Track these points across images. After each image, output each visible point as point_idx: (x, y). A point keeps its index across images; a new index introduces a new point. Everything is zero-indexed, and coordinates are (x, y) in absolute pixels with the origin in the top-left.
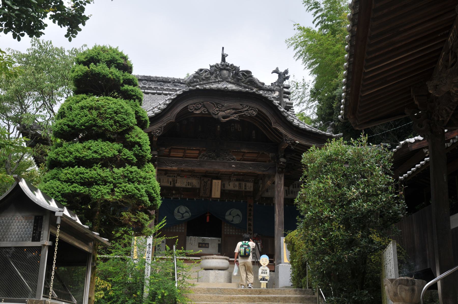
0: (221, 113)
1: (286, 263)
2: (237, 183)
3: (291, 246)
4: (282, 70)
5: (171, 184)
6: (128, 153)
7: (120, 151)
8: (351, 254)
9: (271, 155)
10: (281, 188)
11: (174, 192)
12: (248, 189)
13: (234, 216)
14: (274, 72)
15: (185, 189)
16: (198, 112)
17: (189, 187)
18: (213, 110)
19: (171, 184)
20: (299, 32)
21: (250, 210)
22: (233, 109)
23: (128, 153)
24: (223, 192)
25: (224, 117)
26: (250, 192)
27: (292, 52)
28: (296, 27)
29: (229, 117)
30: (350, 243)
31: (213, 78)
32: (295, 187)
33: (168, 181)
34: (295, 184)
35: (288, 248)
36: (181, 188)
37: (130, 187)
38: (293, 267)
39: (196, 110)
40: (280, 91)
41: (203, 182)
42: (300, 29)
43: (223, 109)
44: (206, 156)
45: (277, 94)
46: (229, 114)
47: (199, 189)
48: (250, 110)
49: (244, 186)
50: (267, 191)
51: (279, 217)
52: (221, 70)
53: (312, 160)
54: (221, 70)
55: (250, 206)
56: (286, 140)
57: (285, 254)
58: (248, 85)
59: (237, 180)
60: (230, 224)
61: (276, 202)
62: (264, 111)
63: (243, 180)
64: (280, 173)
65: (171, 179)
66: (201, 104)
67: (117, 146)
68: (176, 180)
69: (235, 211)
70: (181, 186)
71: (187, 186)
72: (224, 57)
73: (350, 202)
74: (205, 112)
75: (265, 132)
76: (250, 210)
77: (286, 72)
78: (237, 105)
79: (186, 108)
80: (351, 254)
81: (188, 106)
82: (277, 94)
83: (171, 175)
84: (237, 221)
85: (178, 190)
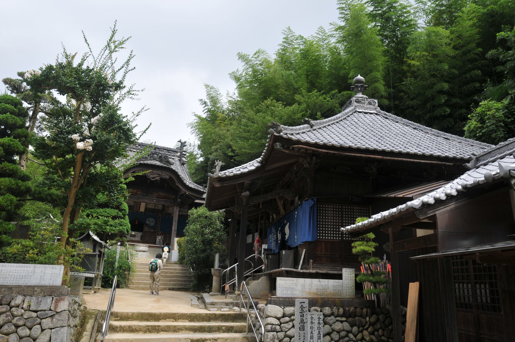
3: (179, 244)
4: (183, 141)
6: (120, 214)
7: (117, 213)
8: (203, 255)
13: (151, 222)
14: (179, 141)
20: (194, 118)
23: (120, 214)
24: (146, 209)
25: (153, 178)
27: (189, 129)
28: (193, 114)
30: (204, 251)
31: (149, 157)
35: (178, 245)
37: (121, 227)
38: (179, 255)
40: (181, 153)
42: (195, 115)
45: (179, 154)
47: (133, 206)
48: (166, 175)
51: (174, 227)
52: (153, 154)
53: (193, 214)
54: (153, 154)
57: (176, 247)
60: (148, 226)
61: (174, 219)
62: (172, 176)
64: (177, 206)
67: (117, 211)
69: (151, 219)
73: (205, 235)
77: (185, 142)
78: (160, 172)
80: (203, 255)
82: (179, 154)
84: (152, 224)
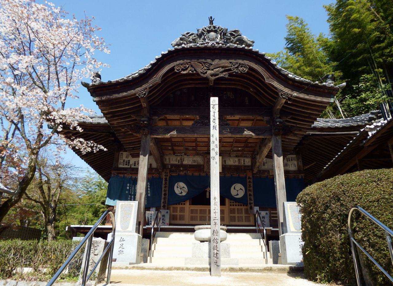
0: (209, 72)
1: (293, 232)
2: (237, 159)
5: (179, 162)
9: (266, 118)
10: (279, 151)
11: (181, 169)
12: (246, 164)
15: (191, 166)
16: (185, 72)
17: (195, 164)
18: (200, 69)
19: (179, 162)
21: (250, 182)
22: (222, 67)
26: (248, 166)
29: (218, 75)
32: (289, 161)
33: (176, 160)
34: (289, 158)
36: (188, 165)
39: (183, 70)
41: (206, 158)
43: (211, 67)
44: (199, 123)
46: (218, 72)
47: (203, 165)
49: (242, 162)
50: (264, 165)
55: (249, 178)
56: (282, 95)
58: (237, 44)
59: (236, 156)
63: (241, 156)
65: (179, 158)
66: (188, 64)
68: (184, 159)
70: (188, 164)
71: (193, 164)
72: (211, 22)
74: (192, 71)
75: (257, 98)
76: (250, 182)
78: (225, 62)
79: (173, 69)
81: (174, 66)
83: (179, 155)
85: (186, 167)
